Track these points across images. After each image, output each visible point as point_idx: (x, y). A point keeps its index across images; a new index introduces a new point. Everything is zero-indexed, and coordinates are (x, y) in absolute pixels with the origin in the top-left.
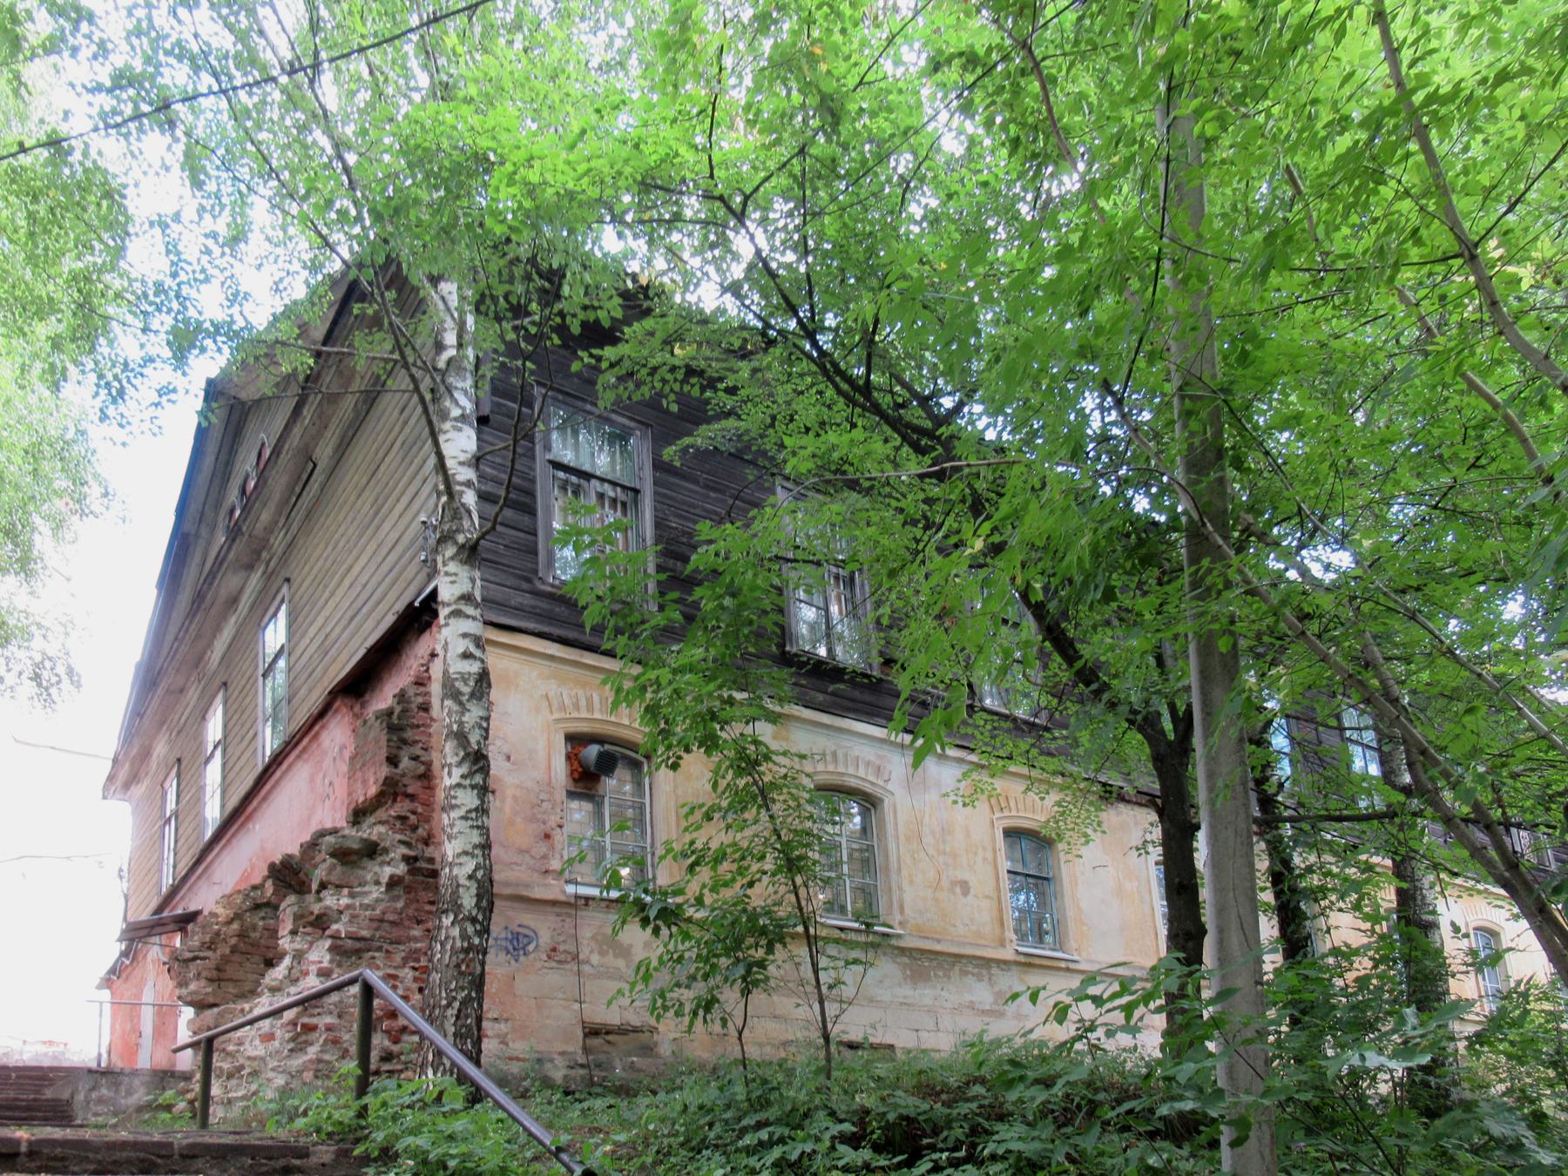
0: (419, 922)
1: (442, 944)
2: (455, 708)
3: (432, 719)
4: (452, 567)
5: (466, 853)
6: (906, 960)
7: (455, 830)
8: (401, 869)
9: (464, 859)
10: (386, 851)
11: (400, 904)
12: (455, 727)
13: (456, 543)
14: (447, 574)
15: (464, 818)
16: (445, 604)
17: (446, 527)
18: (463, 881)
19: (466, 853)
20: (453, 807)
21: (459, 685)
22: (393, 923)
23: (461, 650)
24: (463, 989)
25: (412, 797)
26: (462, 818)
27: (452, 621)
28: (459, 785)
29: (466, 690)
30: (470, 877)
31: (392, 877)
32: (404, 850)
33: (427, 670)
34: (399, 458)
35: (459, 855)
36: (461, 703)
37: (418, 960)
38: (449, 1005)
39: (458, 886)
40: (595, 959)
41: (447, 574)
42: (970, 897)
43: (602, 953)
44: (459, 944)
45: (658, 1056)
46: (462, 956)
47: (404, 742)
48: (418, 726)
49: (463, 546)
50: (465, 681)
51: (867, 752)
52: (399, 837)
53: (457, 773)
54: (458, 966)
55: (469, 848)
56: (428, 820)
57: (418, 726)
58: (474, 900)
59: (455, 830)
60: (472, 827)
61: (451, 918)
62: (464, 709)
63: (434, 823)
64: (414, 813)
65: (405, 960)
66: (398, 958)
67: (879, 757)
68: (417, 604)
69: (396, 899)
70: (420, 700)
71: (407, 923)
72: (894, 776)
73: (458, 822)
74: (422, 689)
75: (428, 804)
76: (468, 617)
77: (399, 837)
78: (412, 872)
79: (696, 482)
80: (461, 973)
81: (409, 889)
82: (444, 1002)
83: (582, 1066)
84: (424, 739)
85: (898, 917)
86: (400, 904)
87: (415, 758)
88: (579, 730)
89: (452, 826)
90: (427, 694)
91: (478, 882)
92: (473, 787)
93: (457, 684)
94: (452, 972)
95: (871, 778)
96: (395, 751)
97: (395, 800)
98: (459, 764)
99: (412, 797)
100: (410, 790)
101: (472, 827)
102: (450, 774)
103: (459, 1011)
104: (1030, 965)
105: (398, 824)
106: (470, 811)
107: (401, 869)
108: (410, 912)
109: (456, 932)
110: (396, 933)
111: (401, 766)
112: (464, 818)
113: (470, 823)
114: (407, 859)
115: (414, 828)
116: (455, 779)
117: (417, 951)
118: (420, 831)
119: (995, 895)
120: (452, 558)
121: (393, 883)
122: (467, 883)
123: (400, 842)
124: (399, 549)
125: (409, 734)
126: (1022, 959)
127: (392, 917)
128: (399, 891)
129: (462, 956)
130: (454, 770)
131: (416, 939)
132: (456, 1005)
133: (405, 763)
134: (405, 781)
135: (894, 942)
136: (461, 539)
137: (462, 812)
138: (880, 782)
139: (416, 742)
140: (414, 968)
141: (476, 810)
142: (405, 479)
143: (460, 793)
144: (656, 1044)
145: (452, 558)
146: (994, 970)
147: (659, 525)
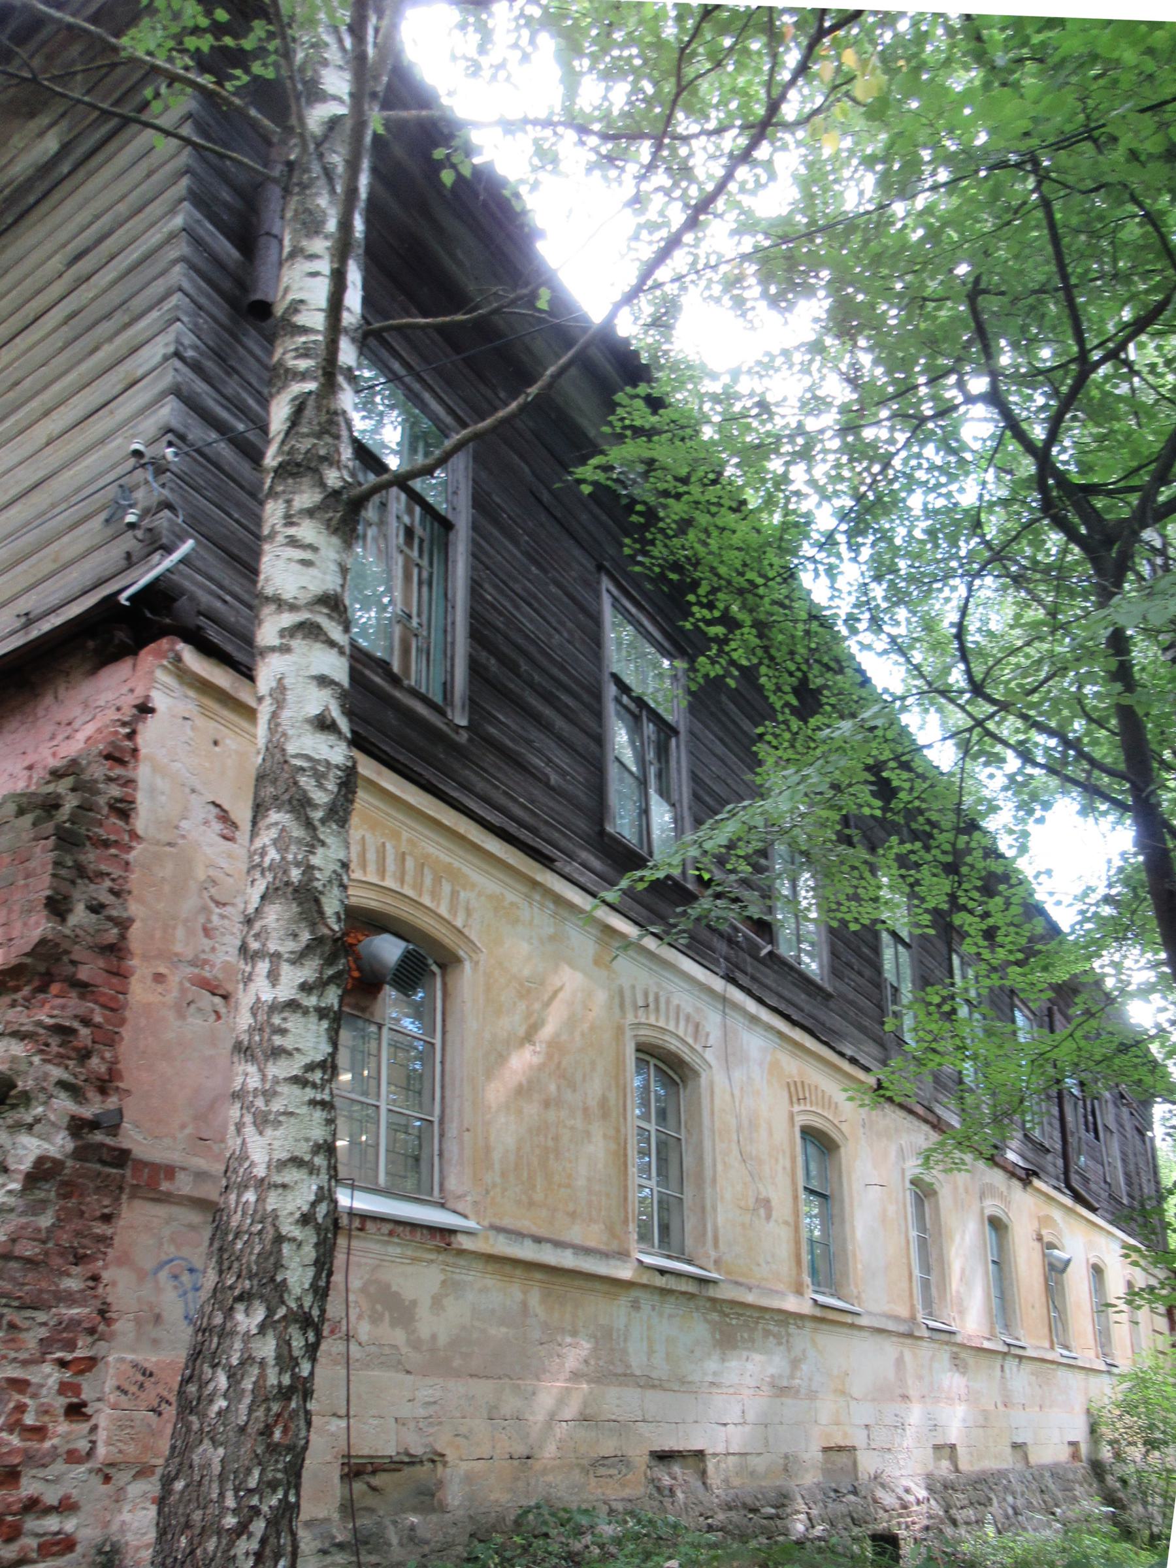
0: (79, 1259)
1: (234, 1376)
2: (298, 832)
3: (134, 835)
4: (307, 531)
5: (296, 1162)
6: (715, 1316)
7: (277, 1106)
8: (59, 1145)
9: (291, 1175)
10: (26, 1099)
11: (45, 1221)
12: (295, 874)
13: (322, 484)
14: (293, 542)
15: (299, 1081)
16: (280, 603)
17: (304, 445)
18: (288, 1228)
19: (296, 1162)
20: (277, 1053)
21: (306, 782)
22: (30, 1263)
23: (314, 710)
24: (273, 1486)
25: (83, 988)
26: (295, 1080)
27: (297, 643)
28: (292, 1005)
29: (321, 797)
30: (306, 1219)
31: (40, 1161)
32: (64, 1104)
33: (131, 736)
34: (58, 340)
35: (282, 1165)
36: (309, 824)
37: (71, 1346)
38: (242, 1529)
39: (279, 1239)
40: (364, 1330)
41: (293, 542)
42: (772, 1224)
43: (375, 1320)
44: (272, 1379)
45: (442, 1509)
46: (276, 1407)
47: (81, 871)
48: (106, 844)
49: (336, 493)
50: (319, 777)
51: (684, 999)
52: (57, 1073)
53: (292, 978)
54: (267, 1431)
55: (303, 1150)
56: (111, 1040)
57: (106, 844)
58: (310, 1273)
59: (277, 1106)
60: (313, 1103)
61: (260, 1314)
62: (315, 843)
63: (123, 1048)
64: (86, 1022)
65: (46, 1344)
66: (31, 1340)
67: (698, 1010)
68: (123, 598)
69: (38, 1208)
70: (115, 791)
71: (57, 1261)
72: (711, 1042)
73: (285, 1089)
74: (118, 771)
75: (115, 1009)
76: (332, 644)
77: (57, 1073)
78: (80, 1154)
79: (516, 543)
80: (273, 1448)
81: (68, 1189)
82: (230, 1521)
83: (341, 1546)
84: (116, 872)
85: (713, 1254)
86: (45, 1221)
87: (96, 908)
88: (373, 904)
89: (269, 1095)
90: (130, 782)
91: (318, 1228)
92: (322, 1013)
93: (303, 780)
94: (250, 1445)
95: (690, 1041)
96: (65, 887)
97: (43, 989)
98: (298, 959)
99: (83, 988)
100: (83, 974)
101: (313, 1103)
102: (273, 977)
103: (263, 1541)
104: (822, 1320)
105: (54, 1041)
106: (310, 1067)
107: (59, 1145)
108: (65, 1239)
109: (267, 1348)
110: (33, 1282)
111: (72, 920)
112: (299, 1081)
113: (310, 1093)
114: (77, 1126)
115: (84, 1055)
116: (286, 991)
117: (74, 1323)
118: (94, 1062)
119: (791, 1220)
120: (310, 513)
121: (42, 1172)
122: (297, 1232)
123: (62, 1084)
124: (39, 500)
125: (91, 857)
126: (818, 1312)
127: (28, 1249)
128: (47, 1191)
129: (276, 1407)
130: (285, 968)
131: (69, 1299)
132: (258, 1527)
133: (79, 915)
134: (78, 953)
135: (712, 1292)
136: (333, 478)
137: (294, 1067)
138: (698, 1047)
139: (102, 875)
140: (63, 1364)
141: (322, 1065)
142: (72, 377)
143: (294, 1023)
144: (440, 1484)
145: (310, 513)
146: (792, 1329)
147: (475, 588)
